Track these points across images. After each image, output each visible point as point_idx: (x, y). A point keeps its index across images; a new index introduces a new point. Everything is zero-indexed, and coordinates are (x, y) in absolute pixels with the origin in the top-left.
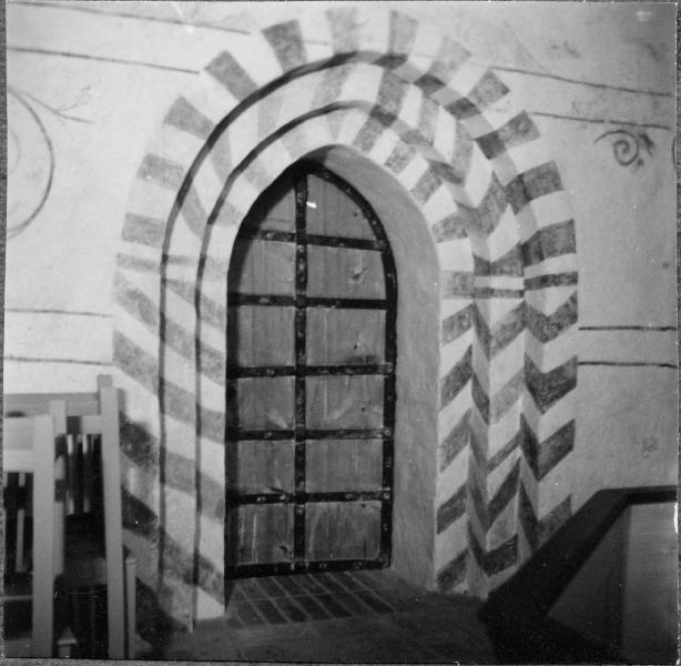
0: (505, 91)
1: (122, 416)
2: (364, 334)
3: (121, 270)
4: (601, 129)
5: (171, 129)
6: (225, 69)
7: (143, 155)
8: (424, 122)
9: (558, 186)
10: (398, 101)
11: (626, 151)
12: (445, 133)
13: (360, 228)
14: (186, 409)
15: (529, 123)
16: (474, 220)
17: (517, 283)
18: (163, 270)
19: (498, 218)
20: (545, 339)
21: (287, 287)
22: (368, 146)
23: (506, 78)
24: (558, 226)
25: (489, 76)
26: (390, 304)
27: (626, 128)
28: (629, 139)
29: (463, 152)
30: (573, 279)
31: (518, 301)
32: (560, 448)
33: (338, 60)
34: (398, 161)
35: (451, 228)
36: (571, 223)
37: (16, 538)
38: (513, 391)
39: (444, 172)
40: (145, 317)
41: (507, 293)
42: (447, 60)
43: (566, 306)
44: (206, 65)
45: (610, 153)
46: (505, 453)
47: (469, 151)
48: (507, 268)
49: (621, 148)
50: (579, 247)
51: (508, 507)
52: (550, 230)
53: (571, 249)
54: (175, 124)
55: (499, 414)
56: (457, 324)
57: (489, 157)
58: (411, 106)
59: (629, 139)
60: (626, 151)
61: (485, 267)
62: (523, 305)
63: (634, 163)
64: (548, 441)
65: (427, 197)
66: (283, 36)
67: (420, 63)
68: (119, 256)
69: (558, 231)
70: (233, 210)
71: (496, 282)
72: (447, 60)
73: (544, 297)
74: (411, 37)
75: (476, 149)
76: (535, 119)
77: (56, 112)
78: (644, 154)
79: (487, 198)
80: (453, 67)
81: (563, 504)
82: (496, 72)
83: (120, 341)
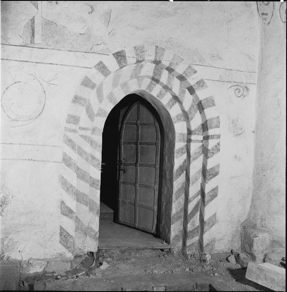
0: (195, 72)
1: (136, 63)
3: (66, 133)
4: (230, 85)
7: (74, 95)
11: (239, 92)
14: (86, 178)
19: (194, 115)
23: (195, 68)
25: (190, 67)
27: (240, 84)
28: (240, 88)
30: (219, 137)
32: (212, 196)
34: (161, 94)
36: (218, 117)
37: (154, 108)
38: (198, 175)
45: (233, 92)
46: (194, 197)
47: (184, 92)
48: (197, 133)
49: (237, 91)
50: (220, 126)
51: (195, 216)
53: (218, 127)
54: (84, 85)
57: (191, 94)
58: (164, 77)
59: (240, 88)
60: (239, 92)
63: (242, 96)
64: (208, 193)
67: (165, 63)
68: (65, 128)
69: (213, 120)
73: (208, 142)
74: (162, 55)
75: (187, 91)
76: (205, 81)
78: (245, 93)
80: (177, 64)
81: (213, 215)
82: (191, 65)
83: (65, 155)
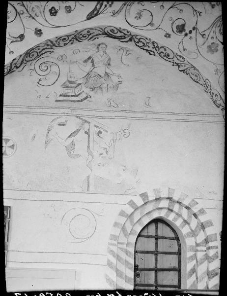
2: (171, 261)
5: (120, 216)
6: (131, 203)
8: (180, 211)
9: (212, 225)
10: (173, 207)
12: (185, 213)
13: (172, 235)
15: (204, 210)
16: (193, 233)
17: (205, 248)
18: (178, 202)
20: (210, 262)
21: (160, 249)
22: (168, 216)
24: (213, 235)
25: (193, 200)
26: (179, 253)
29: (190, 217)
31: (205, 253)
33: (158, 199)
34: (175, 219)
35: (189, 235)
39: (186, 222)
40: (114, 256)
41: (202, 251)
42: (182, 198)
43: (215, 254)
44: (211, 7)
47: (191, 217)
52: (210, 236)
55: (200, 281)
56: (191, 258)
58: (176, 207)
61: (197, 245)
62: (206, 254)
65: (183, 228)
66: (144, 196)
70: (160, 213)
71: (199, 248)
72: (182, 198)
76: (205, 209)
77: (97, 214)
79: (196, 228)
80: (184, 199)
83: (109, 261)
